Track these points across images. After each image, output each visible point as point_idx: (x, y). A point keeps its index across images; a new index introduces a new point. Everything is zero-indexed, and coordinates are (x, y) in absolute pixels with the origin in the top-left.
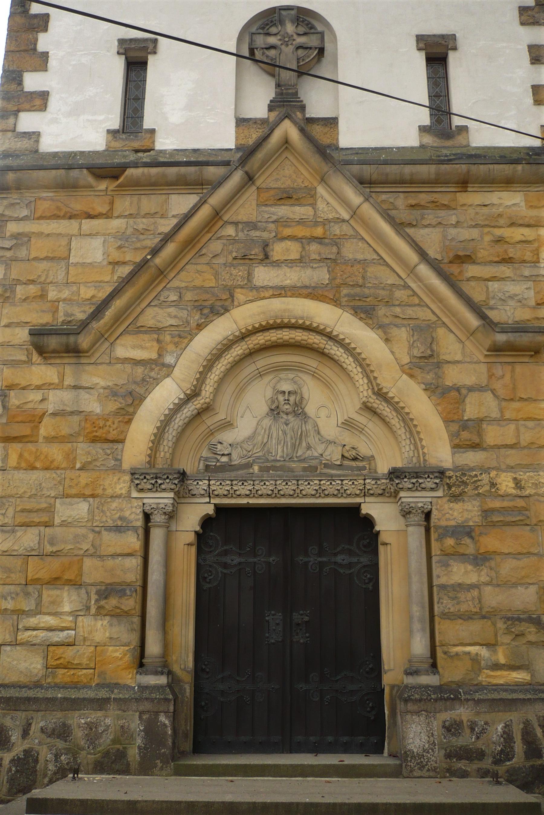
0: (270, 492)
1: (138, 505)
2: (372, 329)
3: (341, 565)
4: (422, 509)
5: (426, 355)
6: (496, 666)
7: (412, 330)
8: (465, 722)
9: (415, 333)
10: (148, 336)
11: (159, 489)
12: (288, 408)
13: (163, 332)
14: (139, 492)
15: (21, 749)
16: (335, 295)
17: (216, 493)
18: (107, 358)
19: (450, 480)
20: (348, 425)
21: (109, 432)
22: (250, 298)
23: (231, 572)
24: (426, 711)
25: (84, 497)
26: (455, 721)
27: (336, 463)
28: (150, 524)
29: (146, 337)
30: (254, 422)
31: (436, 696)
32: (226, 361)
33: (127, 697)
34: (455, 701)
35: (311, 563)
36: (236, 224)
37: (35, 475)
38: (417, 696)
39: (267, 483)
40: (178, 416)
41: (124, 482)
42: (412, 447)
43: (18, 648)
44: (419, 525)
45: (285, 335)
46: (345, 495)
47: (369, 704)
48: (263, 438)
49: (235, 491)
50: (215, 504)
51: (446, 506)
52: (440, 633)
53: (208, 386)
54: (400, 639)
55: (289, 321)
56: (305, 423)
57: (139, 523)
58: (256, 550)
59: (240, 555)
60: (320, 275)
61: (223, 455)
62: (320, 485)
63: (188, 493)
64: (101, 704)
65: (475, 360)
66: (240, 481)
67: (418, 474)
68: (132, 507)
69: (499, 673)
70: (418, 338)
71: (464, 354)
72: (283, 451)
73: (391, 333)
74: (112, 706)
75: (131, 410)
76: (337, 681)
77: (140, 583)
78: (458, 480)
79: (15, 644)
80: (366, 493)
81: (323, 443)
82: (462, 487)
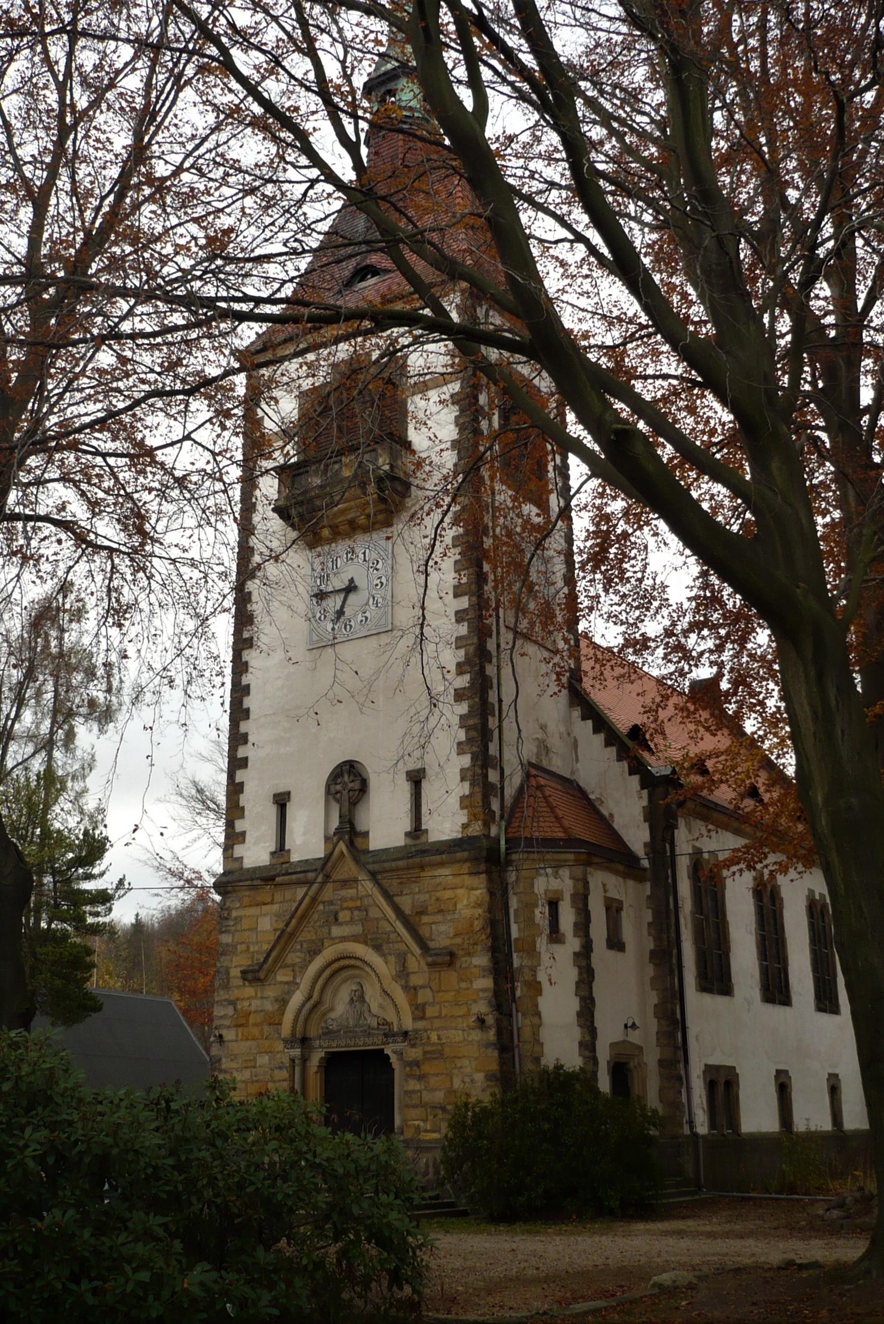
6: (426, 1131)
25: (267, 1053)
36: (324, 903)
37: (248, 1043)
60: (357, 929)
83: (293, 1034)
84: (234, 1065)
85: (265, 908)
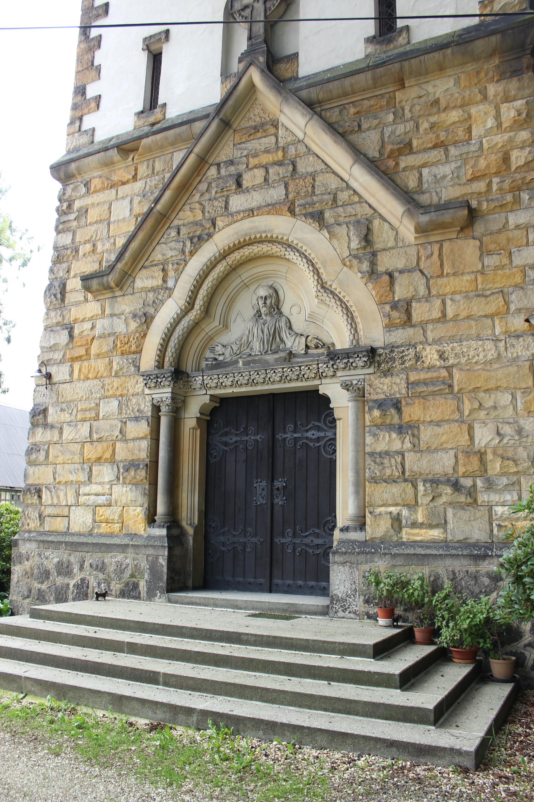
3: (311, 440)
6: (414, 525)
15: (79, 578)
25: (114, 396)
38: (344, 550)
43: (79, 507)
48: (248, 338)
51: (377, 382)
59: (236, 435)
60: (277, 193)
64: (123, 548)
69: (417, 531)
74: (130, 550)
76: (306, 536)
79: (77, 505)
83: (160, 364)
84: (66, 417)
85: (123, 190)
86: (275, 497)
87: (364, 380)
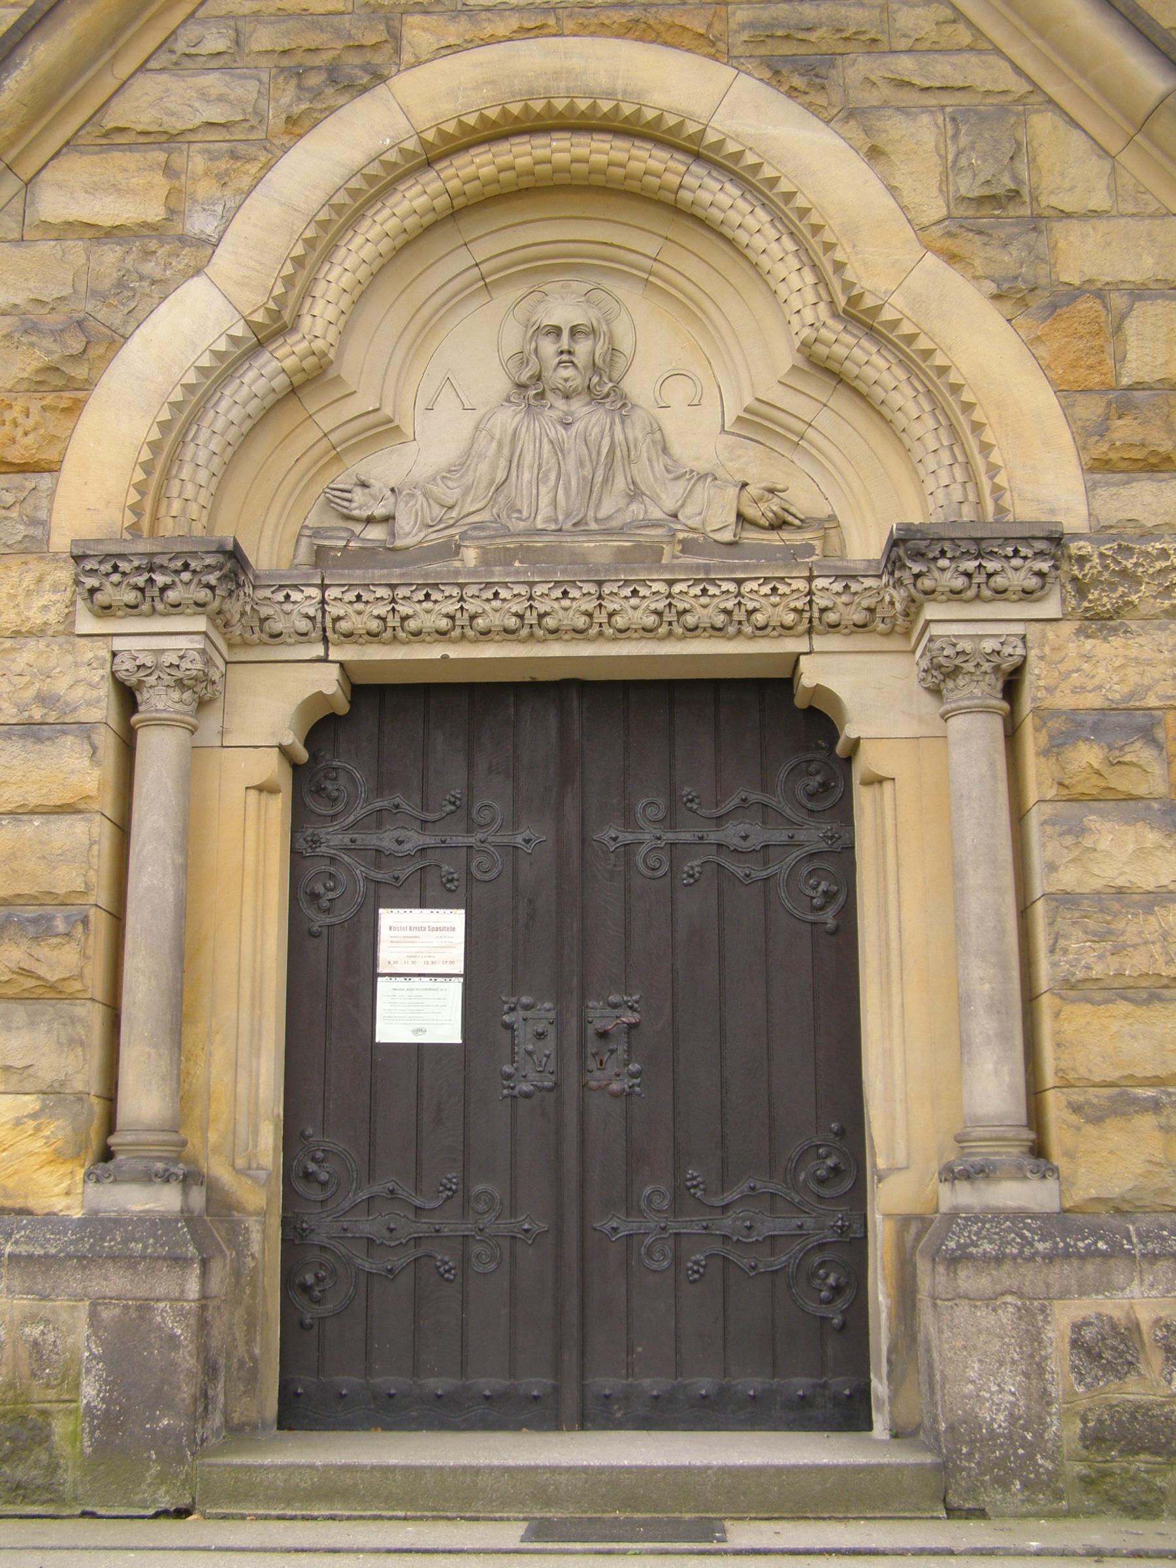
0: (512, 622)
1: (96, 657)
2: (828, 122)
4: (995, 659)
5: (999, 191)
7: (953, 119)
8: (1144, 1328)
9: (964, 129)
10: (137, 155)
11: (160, 606)
12: (572, 378)
13: (185, 146)
14: (98, 616)
16: (710, 26)
17: (343, 626)
18: (13, 225)
19: (1081, 568)
20: (757, 423)
21: (13, 441)
22: (452, 41)
23: (397, 879)
24: (1019, 1294)
26: (1114, 1327)
27: (718, 537)
28: (135, 718)
29: (131, 160)
30: (467, 422)
31: (1048, 1245)
32: (377, 228)
33: (53, 1251)
34: (1112, 1262)
35: (643, 849)
38: (988, 1247)
39: (504, 593)
40: (227, 392)
41: (55, 589)
42: (957, 470)
44: (987, 710)
45: (560, 151)
46: (748, 629)
47: (827, 1275)
48: (494, 467)
49: (405, 619)
50: (342, 664)
51: (1072, 648)
52: (1059, 1045)
53: (320, 303)
54: (923, 1071)
55: (571, 107)
56: (623, 422)
57: (100, 707)
58: (474, 811)
61: (370, 520)
62: (670, 596)
63: (257, 629)
65: (1153, 207)
66: (420, 586)
67: (984, 545)
68: (76, 664)
70: (973, 143)
71: (1114, 190)
72: (554, 503)
73: (886, 131)
75: (79, 372)
76: (725, 1208)
77: (102, 896)
78: (1106, 567)
80: (816, 622)
81: (677, 478)
82: (1121, 589)
86: (592, 1064)
87: (1024, 638)
